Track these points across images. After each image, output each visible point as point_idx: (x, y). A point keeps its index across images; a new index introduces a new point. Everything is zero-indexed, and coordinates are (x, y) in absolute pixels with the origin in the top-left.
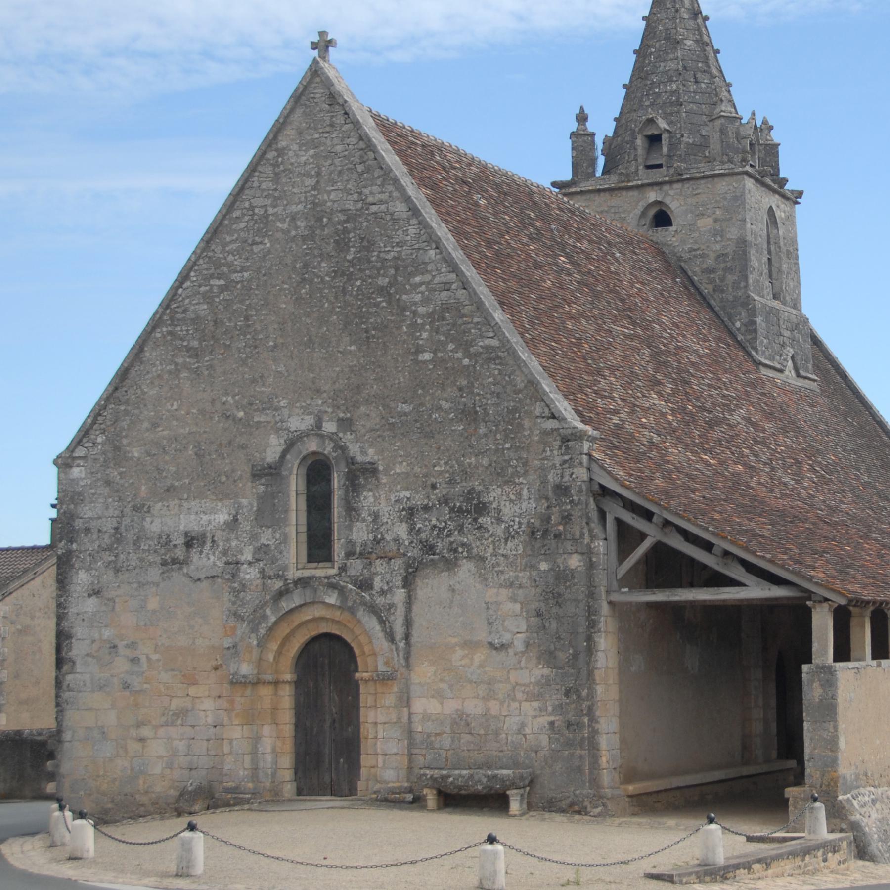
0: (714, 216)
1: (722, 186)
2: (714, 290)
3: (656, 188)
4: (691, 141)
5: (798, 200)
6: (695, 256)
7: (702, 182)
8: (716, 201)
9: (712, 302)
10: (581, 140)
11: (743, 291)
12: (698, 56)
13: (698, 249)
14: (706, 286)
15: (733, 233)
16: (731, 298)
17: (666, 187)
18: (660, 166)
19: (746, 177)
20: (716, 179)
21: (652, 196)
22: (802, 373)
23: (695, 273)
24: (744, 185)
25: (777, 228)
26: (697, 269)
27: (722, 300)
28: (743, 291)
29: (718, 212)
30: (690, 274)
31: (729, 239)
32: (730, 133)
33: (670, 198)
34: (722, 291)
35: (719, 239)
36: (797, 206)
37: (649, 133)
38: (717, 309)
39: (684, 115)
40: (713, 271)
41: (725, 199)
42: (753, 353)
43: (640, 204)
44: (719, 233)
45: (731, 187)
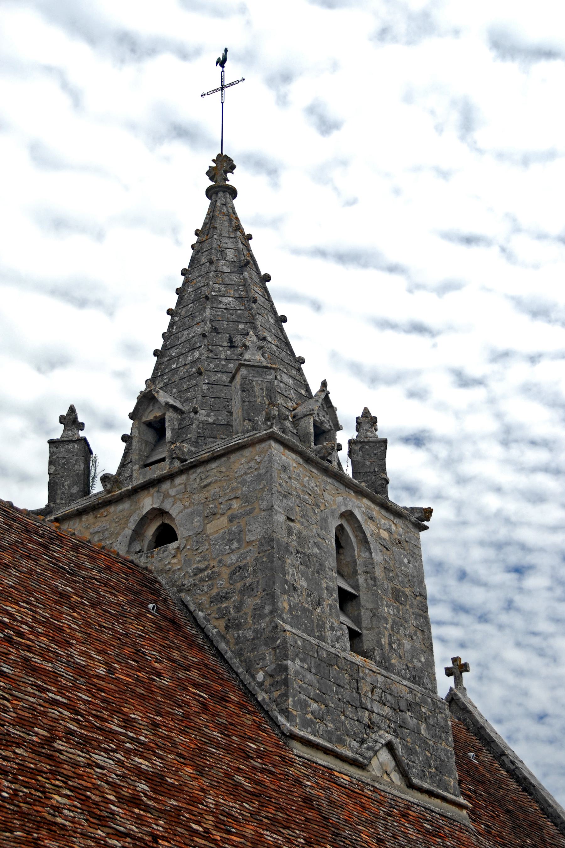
0: (230, 512)
1: (240, 463)
2: (227, 627)
3: (152, 491)
4: (210, 420)
5: (425, 523)
6: (202, 580)
7: (213, 465)
8: (233, 489)
9: (222, 646)
10: (69, 450)
11: (268, 619)
12: (239, 316)
13: (206, 568)
14: (216, 623)
15: (255, 533)
16: (250, 634)
17: (166, 486)
18: (163, 460)
19: (273, 443)
20: (233, 457)
21: (148, 502)
22: (416, 781)
23: (200, 606)
24: (271, 456)
25: (369, 550)
26: (204, 599)
27: (238, 641)
28: (268, 619)
29: (235, 505)
30: (192, 607)
31: (249, 543)
32: (256, 389)
33: (170, 500)
34: (239, 626)
35: (235, 545)
36: (423, 534)
37: (151, 417)
38: (229, 655)
39: (205, 387)
40: (226, 597)
41: (243, 483)
42: (281, 719)
43: (131, 520)
44: (234, 537)
45: (252, 464)
